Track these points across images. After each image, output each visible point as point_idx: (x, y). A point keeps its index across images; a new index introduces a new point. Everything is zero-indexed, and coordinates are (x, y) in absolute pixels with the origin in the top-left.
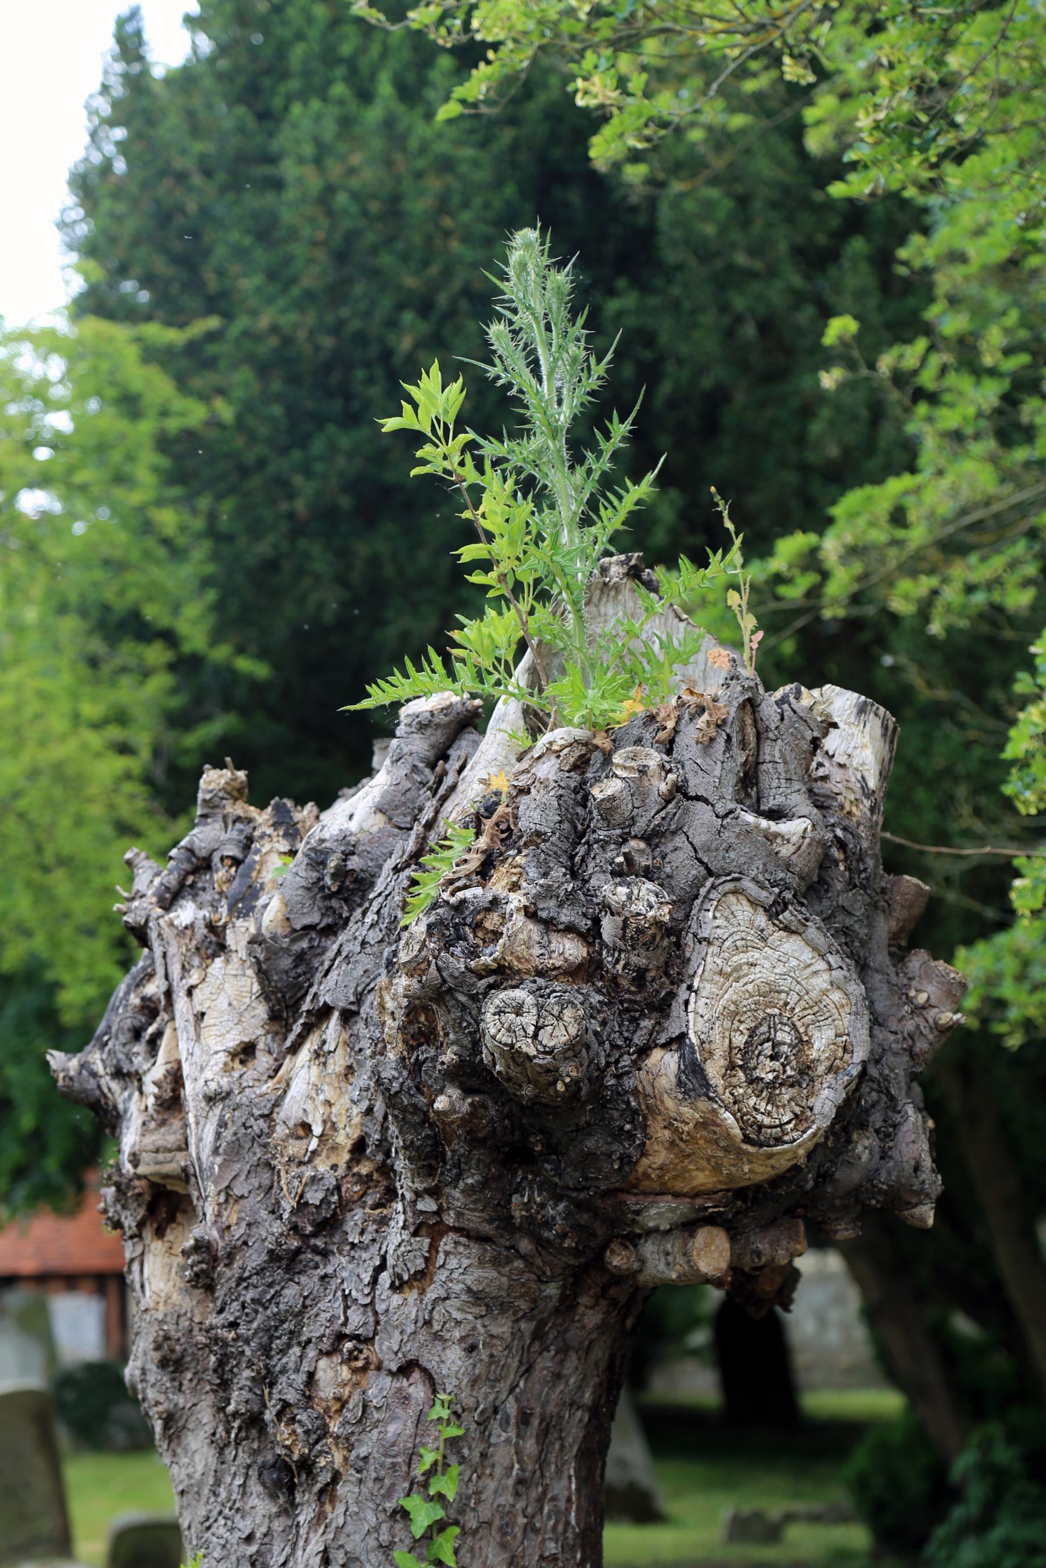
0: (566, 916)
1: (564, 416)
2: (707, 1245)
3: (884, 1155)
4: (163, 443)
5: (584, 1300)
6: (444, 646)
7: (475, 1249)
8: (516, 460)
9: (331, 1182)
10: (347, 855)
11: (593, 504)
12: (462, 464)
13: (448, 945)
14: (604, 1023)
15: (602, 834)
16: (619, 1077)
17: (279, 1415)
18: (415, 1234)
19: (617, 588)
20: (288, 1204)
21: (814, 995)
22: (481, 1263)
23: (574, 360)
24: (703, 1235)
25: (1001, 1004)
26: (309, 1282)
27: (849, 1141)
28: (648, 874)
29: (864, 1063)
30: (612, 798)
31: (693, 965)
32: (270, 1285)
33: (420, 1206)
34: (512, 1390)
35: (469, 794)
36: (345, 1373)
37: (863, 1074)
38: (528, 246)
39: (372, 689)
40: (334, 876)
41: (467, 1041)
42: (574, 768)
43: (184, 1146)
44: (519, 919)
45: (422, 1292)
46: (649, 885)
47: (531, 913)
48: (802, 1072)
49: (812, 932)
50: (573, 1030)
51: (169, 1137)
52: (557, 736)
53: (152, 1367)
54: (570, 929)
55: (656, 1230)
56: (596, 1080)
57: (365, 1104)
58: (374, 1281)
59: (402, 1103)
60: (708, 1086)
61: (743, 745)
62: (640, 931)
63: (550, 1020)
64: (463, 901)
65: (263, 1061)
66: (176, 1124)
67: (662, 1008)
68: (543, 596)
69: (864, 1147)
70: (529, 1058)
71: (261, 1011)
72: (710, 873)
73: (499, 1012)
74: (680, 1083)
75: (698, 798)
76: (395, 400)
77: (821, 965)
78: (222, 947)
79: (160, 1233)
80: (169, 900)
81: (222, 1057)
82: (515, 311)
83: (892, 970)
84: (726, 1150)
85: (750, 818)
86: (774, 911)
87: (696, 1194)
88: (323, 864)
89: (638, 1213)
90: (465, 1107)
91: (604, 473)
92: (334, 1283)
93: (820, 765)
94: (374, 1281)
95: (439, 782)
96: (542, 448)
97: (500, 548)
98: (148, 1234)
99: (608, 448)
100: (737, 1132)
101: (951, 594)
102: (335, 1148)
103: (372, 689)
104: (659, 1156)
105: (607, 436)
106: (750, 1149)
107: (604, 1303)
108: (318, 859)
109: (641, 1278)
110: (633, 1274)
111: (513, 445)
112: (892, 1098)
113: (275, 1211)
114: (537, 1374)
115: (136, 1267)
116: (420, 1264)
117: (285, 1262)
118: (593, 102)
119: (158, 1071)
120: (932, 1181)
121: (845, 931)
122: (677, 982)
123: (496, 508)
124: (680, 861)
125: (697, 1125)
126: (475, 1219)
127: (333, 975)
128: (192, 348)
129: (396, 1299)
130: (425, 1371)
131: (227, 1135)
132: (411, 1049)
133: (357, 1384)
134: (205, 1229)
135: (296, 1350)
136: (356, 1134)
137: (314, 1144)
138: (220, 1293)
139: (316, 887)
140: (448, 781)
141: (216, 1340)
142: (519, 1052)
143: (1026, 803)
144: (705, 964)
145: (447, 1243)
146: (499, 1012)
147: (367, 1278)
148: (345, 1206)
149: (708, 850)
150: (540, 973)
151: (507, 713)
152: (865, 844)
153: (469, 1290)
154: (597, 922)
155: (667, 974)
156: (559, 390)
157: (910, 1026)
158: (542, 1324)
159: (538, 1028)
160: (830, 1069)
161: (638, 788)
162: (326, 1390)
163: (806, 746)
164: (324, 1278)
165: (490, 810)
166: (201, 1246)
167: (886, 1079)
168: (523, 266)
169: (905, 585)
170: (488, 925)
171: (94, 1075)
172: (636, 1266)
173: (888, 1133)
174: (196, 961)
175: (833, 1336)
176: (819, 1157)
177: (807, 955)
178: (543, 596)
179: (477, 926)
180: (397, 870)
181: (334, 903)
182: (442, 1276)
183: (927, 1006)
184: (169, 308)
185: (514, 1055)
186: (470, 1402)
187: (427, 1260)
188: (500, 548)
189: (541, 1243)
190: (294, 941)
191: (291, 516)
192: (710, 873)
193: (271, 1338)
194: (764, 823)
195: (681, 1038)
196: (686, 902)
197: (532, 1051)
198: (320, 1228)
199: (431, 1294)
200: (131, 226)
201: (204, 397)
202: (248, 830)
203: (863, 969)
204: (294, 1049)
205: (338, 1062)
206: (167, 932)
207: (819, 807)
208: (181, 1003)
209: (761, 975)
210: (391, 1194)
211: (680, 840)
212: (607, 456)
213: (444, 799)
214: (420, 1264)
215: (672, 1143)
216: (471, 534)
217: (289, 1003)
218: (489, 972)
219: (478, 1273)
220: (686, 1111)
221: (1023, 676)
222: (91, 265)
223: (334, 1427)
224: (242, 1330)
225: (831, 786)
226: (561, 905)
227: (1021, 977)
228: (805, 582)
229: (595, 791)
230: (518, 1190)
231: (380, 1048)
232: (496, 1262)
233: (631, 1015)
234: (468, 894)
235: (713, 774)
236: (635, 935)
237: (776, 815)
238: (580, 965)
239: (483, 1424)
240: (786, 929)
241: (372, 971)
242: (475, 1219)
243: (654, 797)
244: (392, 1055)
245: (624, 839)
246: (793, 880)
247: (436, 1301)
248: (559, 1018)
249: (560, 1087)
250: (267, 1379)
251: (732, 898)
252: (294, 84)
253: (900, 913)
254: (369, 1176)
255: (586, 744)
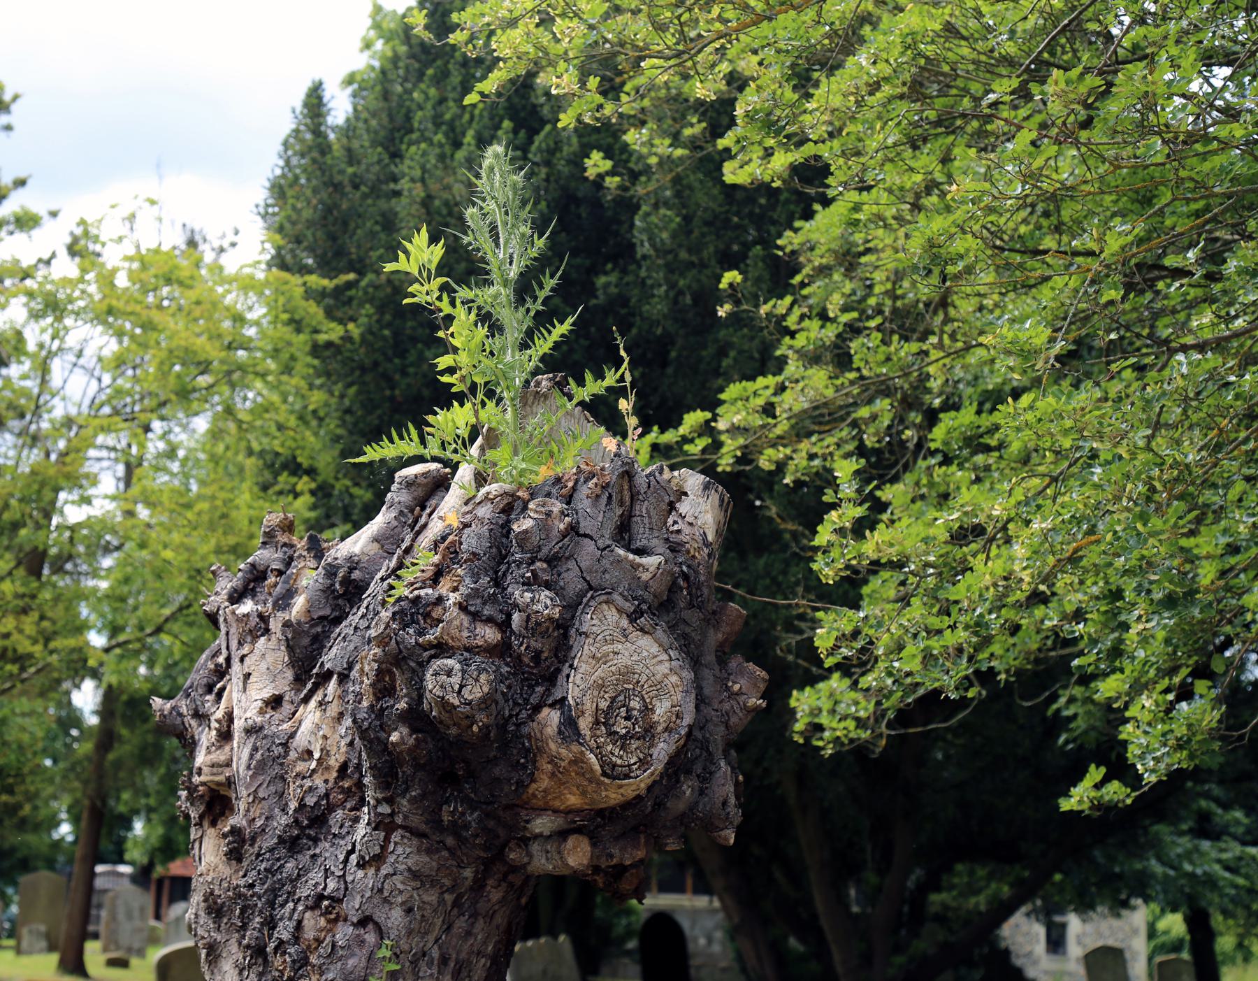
0: (487, 611)
1: (514, 272)
2: (575, 847)
3: (702, 792)
4: (316, 350)
5: (490, 882)
6: (421, 424)
7: (415, 842)
8: (480, 302)
9: (322, 791)
10: (351, 569)
11: (530, 334)
12: (440, 299)
13: (404, 627)
14: (509, 687)
15: (517, 556)
16: (518, 725)
17: (276, 949)
18: (375, 829)
19: (545, 396)
20: (293, 805)
21: (658, 677)
22: (419, 851)
23: (523, 235)
24: (571, 841)
25: (819, 728)
26: (304, 859)
27: (678, 781)
28: (548, 585)
29: (690, 727)
30: (526, 532)
31: (575, 650)
32: (278, 860)
33: (379, 810)
34: (436, 941)
35: (435, 528)
36: (322, 922)
37: (689, 734)
38: (496, 156)
39: (368, 449)
40: (341, 583)
41: (415, 695)
42: (503, 511)
43: (228, 764)
44: (455, 611)
45: (378, 870)
46: (547, 593)
47: (462, 607)
48: (646, 731)
49: (659, 632)
50: (486, 689)
51: (220, 756)
52: (493, 488)
53: (202, 913)
54: (489, 620)
55: (540, 835)
56: (502, 726)
57: (348, 739)
58: (346, 861)
59: (370, 734)
60: (579, 734)
61: (621, 503)
62: (538, 624)
63: (470, 681)
64: (418, 597)
65: (287, 708)
66: (227, 748)
67: (551, 679)
68: (490, 394)
69: (688, 789)
70: (455, 707)
71: (289, 675)
72: (591, 588)
73: (436, 674)
74: (560, 732)
75: (586, 536)
76: (393, 251)
77: (665, 657)
78: (267, 631)
79: (213, 824)
80: (236, 597)
81: (259, 703)
82: (484, 200)
83: (717, 668)
84: (590, 782)
85: (621, 552)
86: (633, 617)
87: (569, 811)
88: (335, 574)
89: (528, 822)
90: (411, 741)
91: (538, 313)
92: (320, 860)
93: (675, 522)
94: (346, 861)
95: (416, 521)
96: (496, 295)
97: (463, 359)
98: (206, 824)
99: (542, 295)
100: (597, 768)
101: (800, 460)
102: (328, 768)
103: (368, 449)
104: (544, 782)
105: (541, 287)
106: (607, 781)
107: (504, 885)
108: (331, 571)
109: (529, 868)
110: (524, 866)
111: (479, 292)
112: (710, 754)
113: (284, 810)
114: (455, 930)
115: (197, 845)
116: (377, 850)
117: (291, 844)
118: (562, 92)
119: (219, 714)
120: (736, 815)
121: (685, 636)
122: (563, 662)
123: (463, 332)
124: (571, 579)
125: (571, 762)
126: (416, 821)
127: (334, 650)
128: (338, 292)
129: (360, 874)
130: (377, 924)
131: (258, 756)
132: (378, 700)
133: (330, 930)
134: (237, 820)
135: (291, 905)
136: (342, 759)
137: (314, 765)
138: (245, 864)
139: (328, 591)
140: (422, 521)
141: (240, 895)
142: (448, 703)
143: (827, 576)
144: (583, 653)
145: (396, 836)
146: (436, 674)
147: (341, 858)
148: (331, 808)
149: (590, 572)
150: (467, 649)
151: (465, 473)
152: (702, 578)
153: (409, 870)
154: (509, 616)
155: (556, 656)
156: (511, 257)
157: (727, 706)
158: (460, 896)
159: (462, 686)
160: (666, 729)
161: (544, 525)
162: (309, 934)
163: (664, 506)
164: (314, 856)
165: (444, 538)
166: (235, 831)
167: (707, 740)
168: (491, 169)
169: (770, 452)
170: (434, 615)
171: (180, 715)
172: (526, 860)
173: (706, 778)
174: (249, 639)
175: (716, 948)
176: (657, 791)
177: (655, 649)
178: (490, 394)
179: (427, 616)
180: (383, 579)
181: (340, 602)
182: (392, 859)
183: (740, 693)
184: (326, 266)
185: (443, 703)
186: (406, 947)
187: (382, 847)
188: (463, 359)
189: (461, 840)
190: (312, 626)
191: (392, 399)
192: (591, 588)
193: (276, 896)
194: (631, 556)
195: (564, 699)
196: (572, 607)
197: (456, 702)
198: (312, 824)
199: (384, 871)
200: (307, 214)
201: (341, 322)
202: (290, 552)
203: (695, 663)
204: (306, 700)
205: (333, 710)
206: (230, 617)
207: (672, 550)
208: (236, 666)
209: (622, 660)
210: (362, 802)
211: (571, 564)
212: (540, 301)
213: (418, 533)
214: (377, 850)
215: (553, 774)
216: (446, 348)
217: (306, 668)
218: (431, 646)
219: (417, 858)
220: (563, 751)
221: (829, 491)
222: (278, 237)
223: (313, 959)
224: (257, 889)
225: (683, 538)
226: (484, 604)
227: (833, 712)
228: (702, 443)
229: (515, 527)
230: (447, 802)
231: (359, 697)
232: (429, 852)
233: (529, 683)
234: (422, 592)
235: (595, 517)
236: (534, 626)
237: (641, 552)
238: (496, 646)
239: (414, 963)
240: (642, 630)
241: (355, 644)
242: (416, 821)
243: (555, 532)
244: (365, 704)
245: (532, 561)
246: (650, 598)
247: (386, 876)
248: (477, 680)
249: (475, 728)
250: (271, 924)
251: (605, 606)
252: (414, 136)
253: (725, 628)
254: (349, 788)
255: (512, 495)
